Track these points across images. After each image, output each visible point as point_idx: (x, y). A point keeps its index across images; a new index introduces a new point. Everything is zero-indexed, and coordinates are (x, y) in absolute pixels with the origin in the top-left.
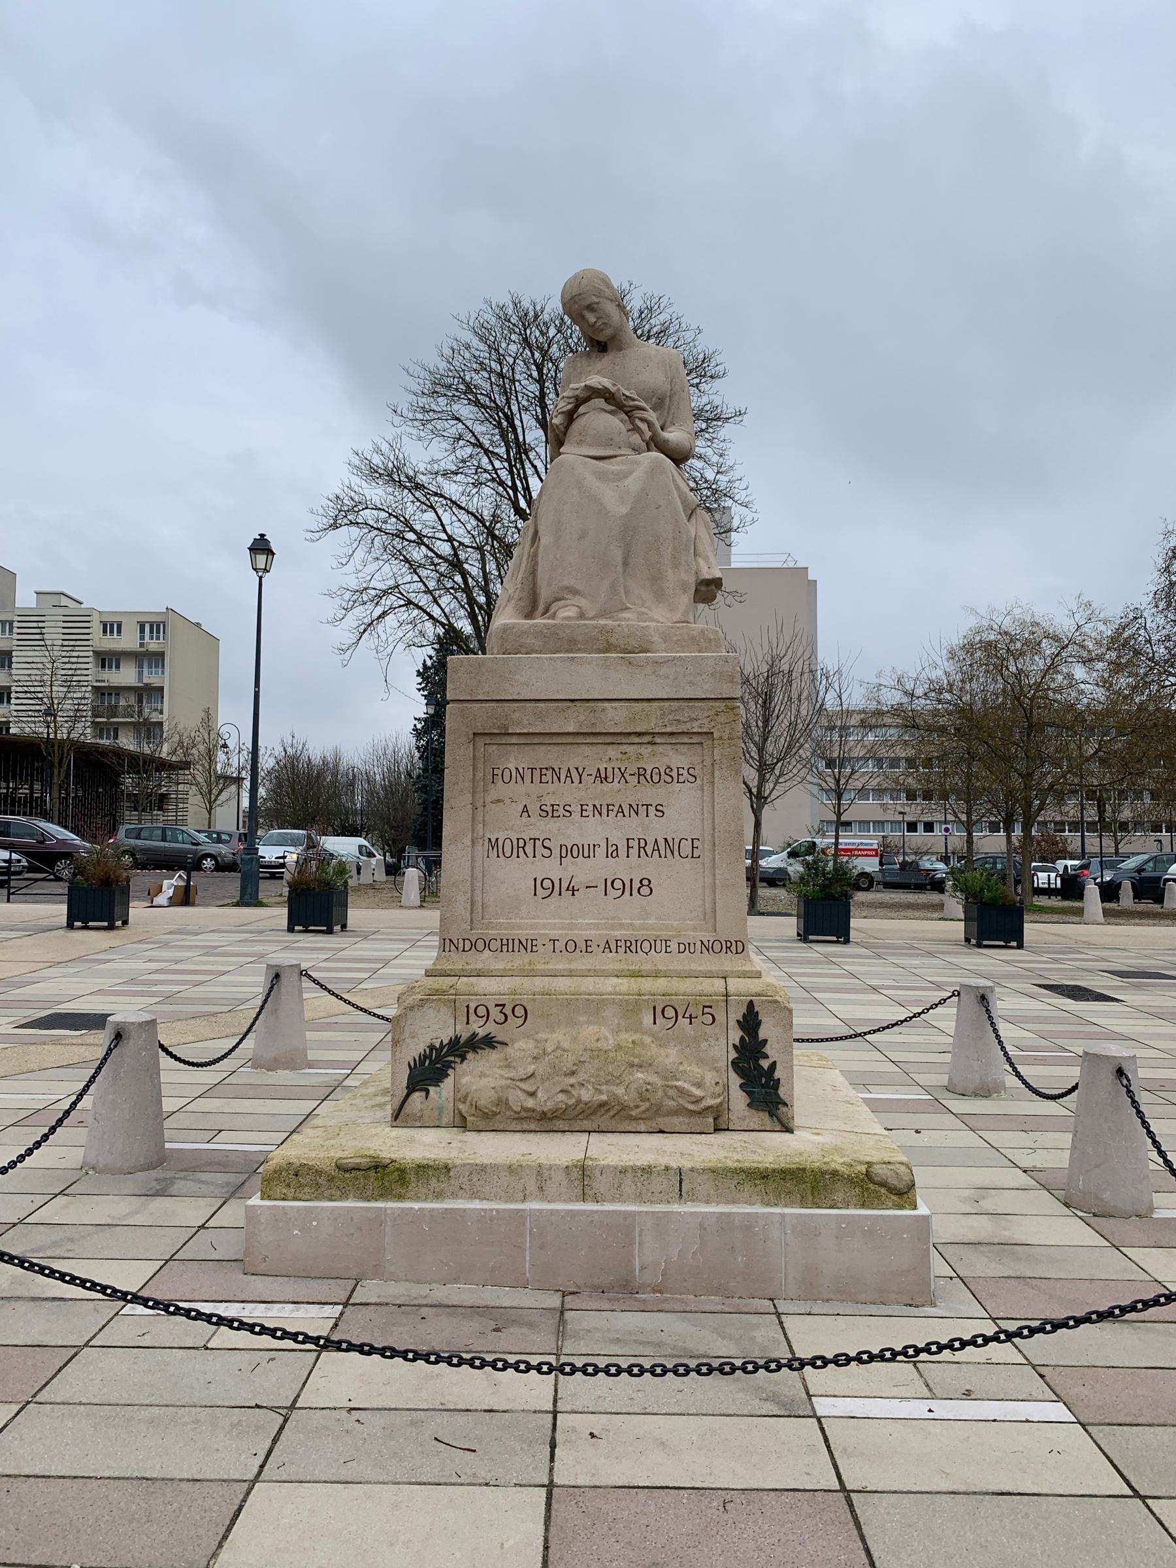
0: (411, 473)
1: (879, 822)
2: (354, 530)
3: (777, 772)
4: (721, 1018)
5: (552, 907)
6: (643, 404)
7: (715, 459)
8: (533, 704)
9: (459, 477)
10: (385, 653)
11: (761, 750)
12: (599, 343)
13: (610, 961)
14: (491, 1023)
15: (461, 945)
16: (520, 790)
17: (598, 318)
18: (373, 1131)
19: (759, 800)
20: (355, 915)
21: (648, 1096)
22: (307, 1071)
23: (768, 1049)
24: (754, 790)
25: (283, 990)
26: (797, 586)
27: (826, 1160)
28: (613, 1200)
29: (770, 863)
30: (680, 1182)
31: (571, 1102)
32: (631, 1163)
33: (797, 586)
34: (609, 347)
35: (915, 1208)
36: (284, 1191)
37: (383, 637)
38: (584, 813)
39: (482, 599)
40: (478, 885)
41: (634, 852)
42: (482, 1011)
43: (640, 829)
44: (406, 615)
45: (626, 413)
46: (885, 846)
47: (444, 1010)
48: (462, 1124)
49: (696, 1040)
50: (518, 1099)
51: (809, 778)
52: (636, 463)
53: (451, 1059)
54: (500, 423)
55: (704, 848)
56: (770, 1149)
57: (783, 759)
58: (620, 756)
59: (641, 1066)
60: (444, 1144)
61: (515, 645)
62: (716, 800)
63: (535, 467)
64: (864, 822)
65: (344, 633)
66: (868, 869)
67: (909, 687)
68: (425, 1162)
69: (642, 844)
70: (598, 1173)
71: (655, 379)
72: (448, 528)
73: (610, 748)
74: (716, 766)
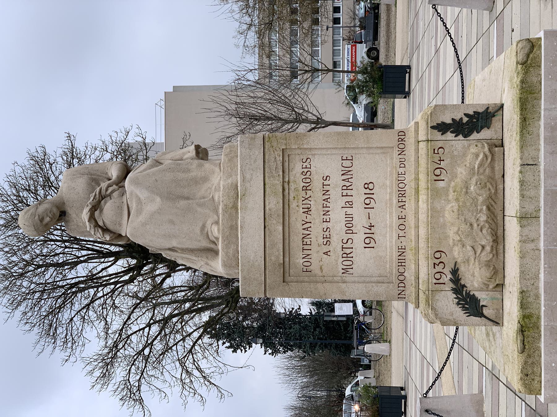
0: (106, 351)
1: (333, 43)
2: (144, 388)
3: (301, 111)
4: (440, 144)
5: (380, 238)
6: (98, 189)
7: (97, 153)
10: (223, 368)
11: (287, 122)
12: (60, 216)
13: (410, 205)
14: (445, 271)
15: (402, 288)
16: (316, 256)
17: (47, 216)
18: (505, 336)
19: (320, 123)
20: (395, 382)
21: (483, 183)
22: (484, 393)
23: (457, 118)
24: (313, 126)
25: (435, 407)
26: (177, 100)
27: (516, 86)
28: (539, 201)
29: (361, 116)
30: (529, 165)
32: (518, 192)
33: (177, 100)
34: (62, 210)
35: (540, 38)
36: (536, 382)
37: (213, 369)
39: (187, 305)
40: (368, 279)
41: (349, 193)
42: (438, 276)
43: (337, 189)
44: (199, 354)
45: (103, 199)
46: (349, 39)
47: (437, 297)
48: (501, 286)
50: (486, 256)
51: (304, 90)
52: (131, 194)
53: (464, 292)
54: (73, 293)
56: (511, 115)
57: (293, 107)
58: (296, 201)
60: (511, 296)
61: (233, 261)
62: (321, 147)
63: (103, 269)
64: (333, 53)
65: (211, 395)
66: (365, 50)
67: (245, 27)
68: (519, 304)
69: (345, 188)
70: (524, 210)
71: (81, 184)
72: (142, 326)
74: (302, 147)
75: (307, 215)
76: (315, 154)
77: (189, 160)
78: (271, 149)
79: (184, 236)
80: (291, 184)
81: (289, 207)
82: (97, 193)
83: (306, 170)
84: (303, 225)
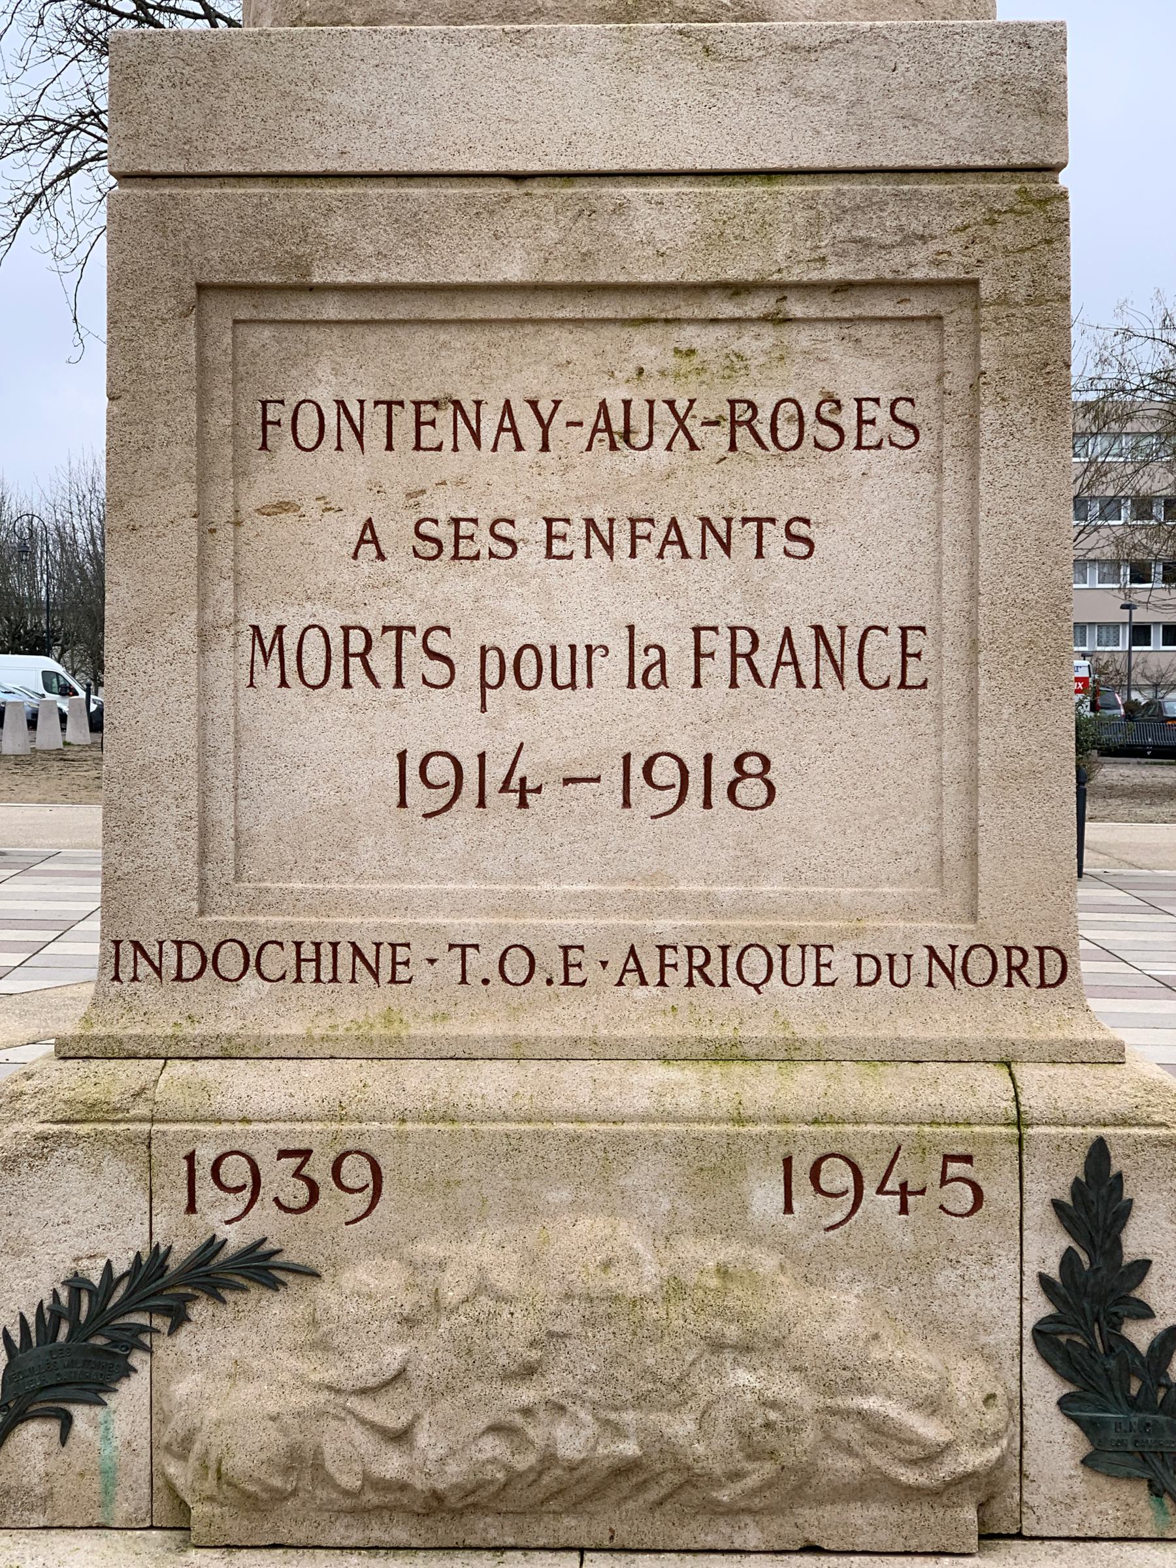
4: (1001, 1191)
5: (457, 842)
8: (390, 190)
10: (72, 260)
13: (641, 1012)
14: (265, 1210)
15: (170, 961)
21: (771, 1440)
23: (1151, 1291)
31: (525, 1461)
37: (68, 223)
38: (558, 547)
40: (222, 772)
41: (716, 669)
42: (236, 1171)
43: (735, 598)
47: (113, 1167)
49: (921, 1263)
50: (351, 1452)
53: (141, 1319)
55: (939, 657)
58: (671, 361)
59: (748, 1349)
62: (984, 505)
69: (744, 645)
73: (639, 336)
74: (987, 395)
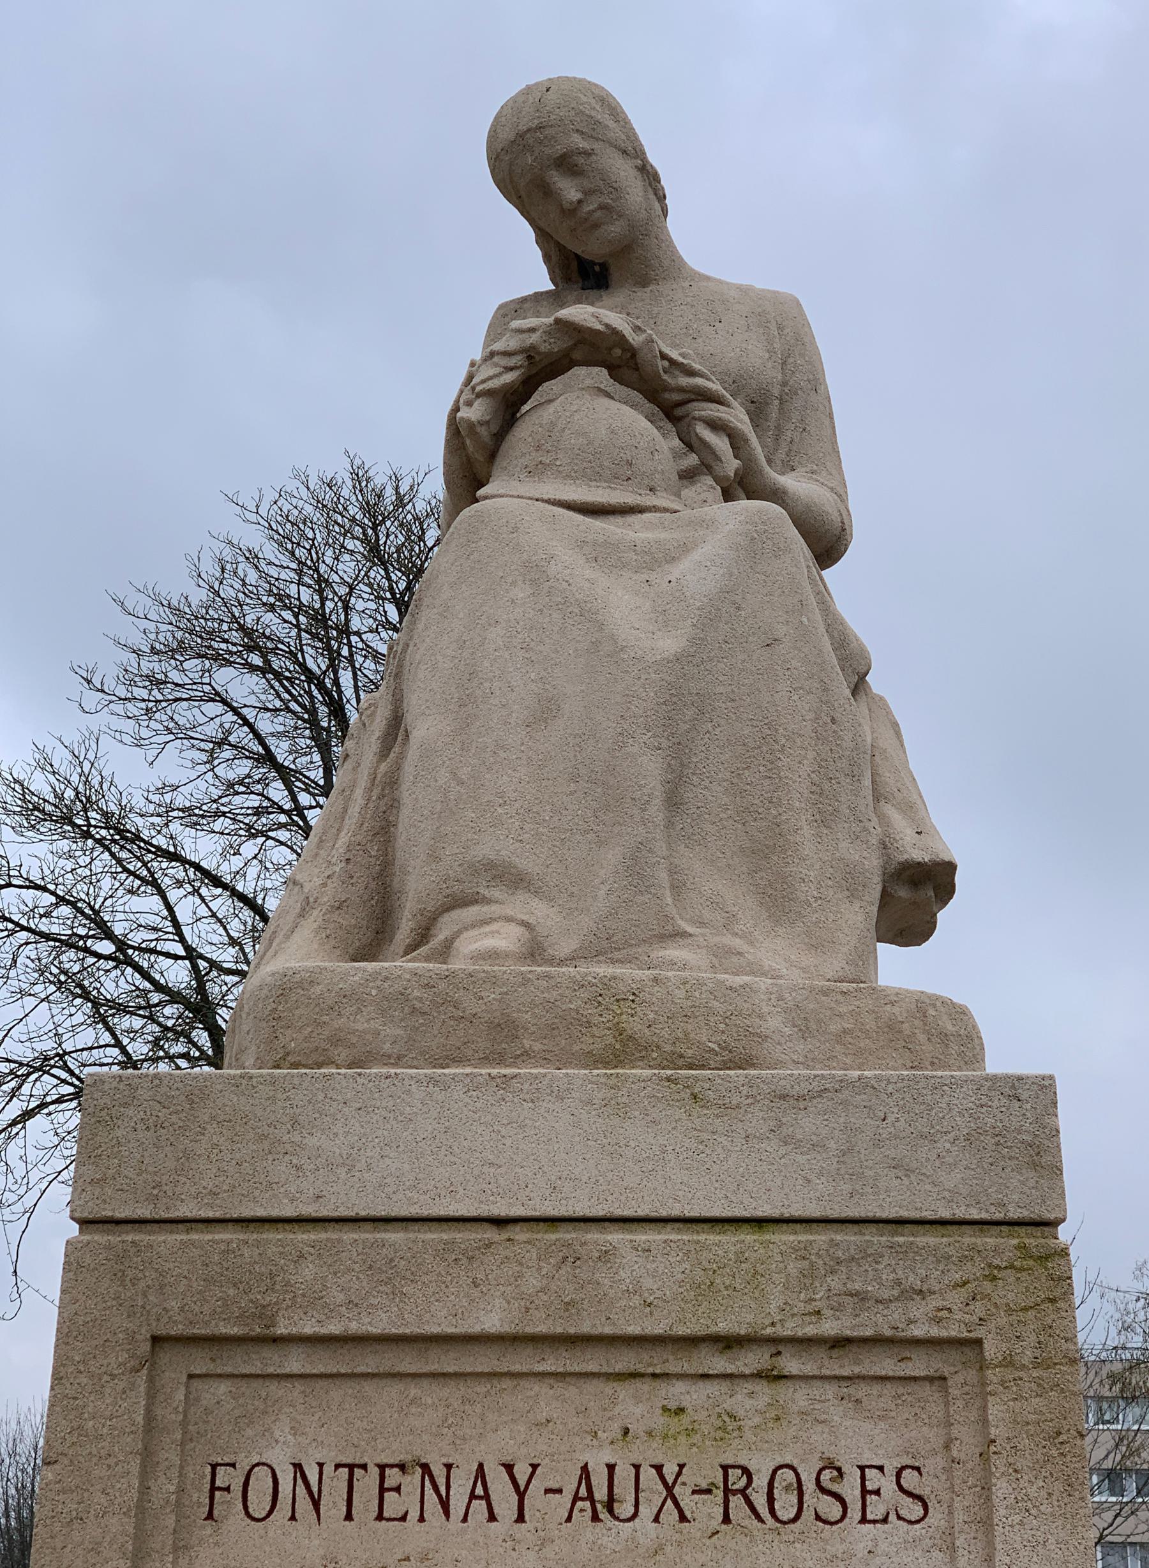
8: (366, 1235)
9: (220, 824)
10: (19, 1208)
17: (588, 193)
37: (19, 1170)
54: (313, 712)
58: (659, 1421)
73: (624, 1391)
74: (999, 1464)
75: (567, 1498)
76: (953, 1548)
77: (876, 831)
78: (974, 1269)
79: (464, 773)
80: (764, 1392)
81: (620, 1377)
82: (699, 381)
83: (850, 1489)
84: (509, 1468)
